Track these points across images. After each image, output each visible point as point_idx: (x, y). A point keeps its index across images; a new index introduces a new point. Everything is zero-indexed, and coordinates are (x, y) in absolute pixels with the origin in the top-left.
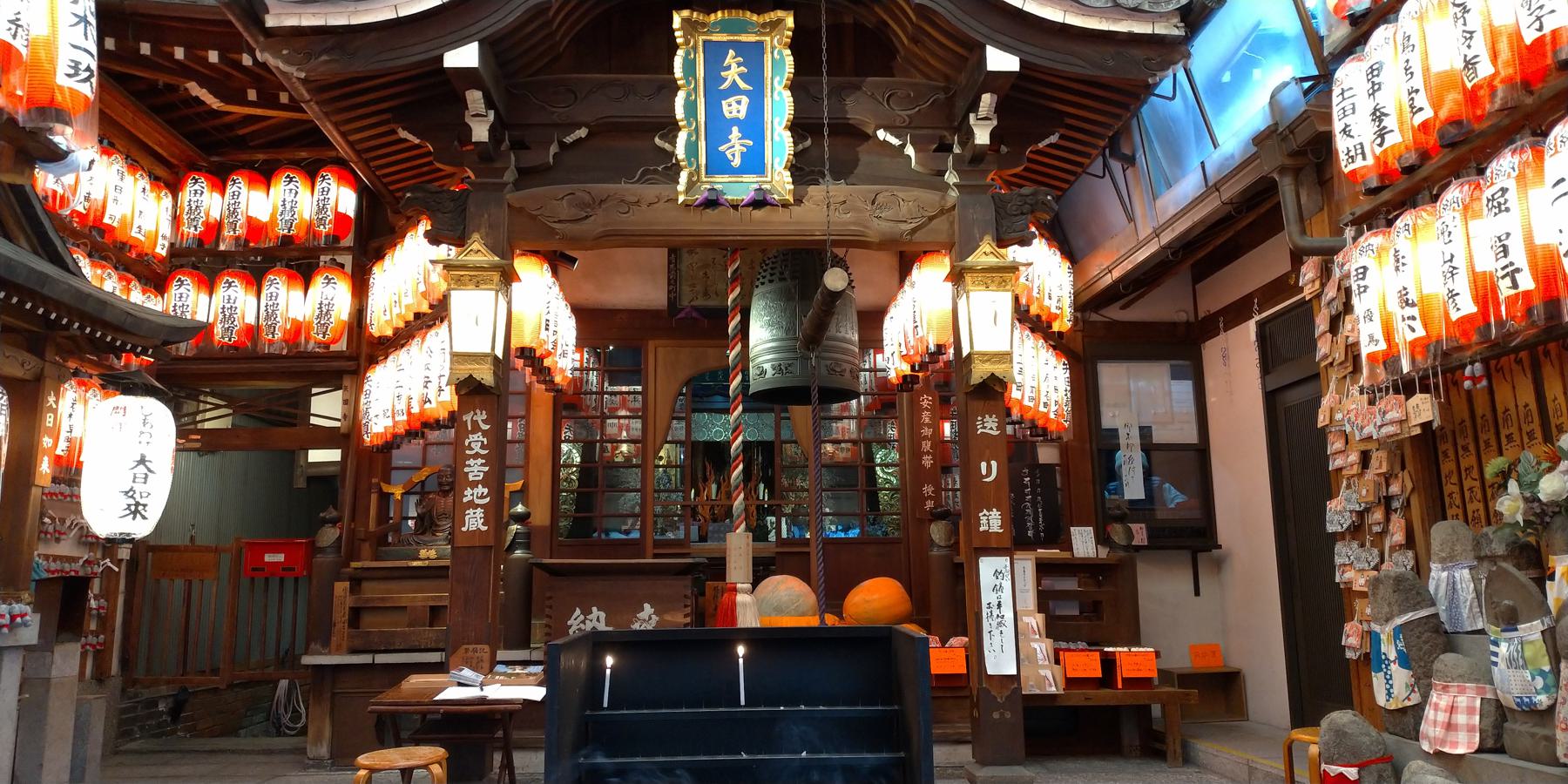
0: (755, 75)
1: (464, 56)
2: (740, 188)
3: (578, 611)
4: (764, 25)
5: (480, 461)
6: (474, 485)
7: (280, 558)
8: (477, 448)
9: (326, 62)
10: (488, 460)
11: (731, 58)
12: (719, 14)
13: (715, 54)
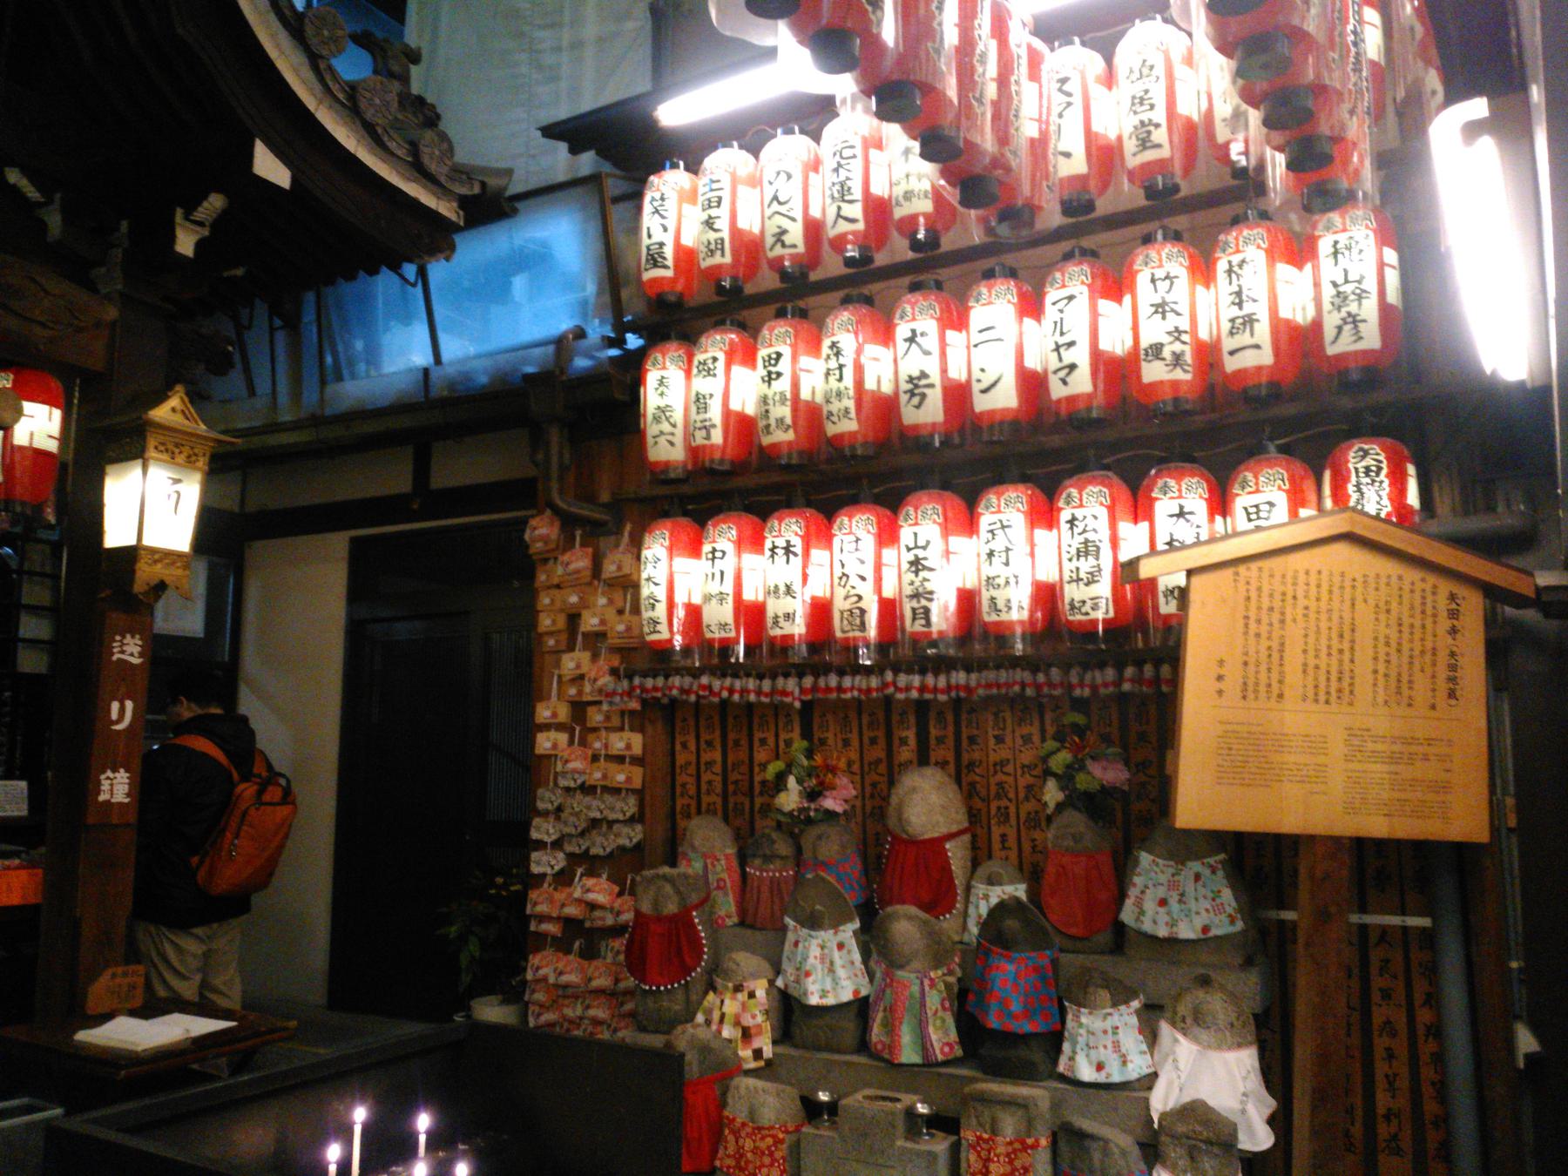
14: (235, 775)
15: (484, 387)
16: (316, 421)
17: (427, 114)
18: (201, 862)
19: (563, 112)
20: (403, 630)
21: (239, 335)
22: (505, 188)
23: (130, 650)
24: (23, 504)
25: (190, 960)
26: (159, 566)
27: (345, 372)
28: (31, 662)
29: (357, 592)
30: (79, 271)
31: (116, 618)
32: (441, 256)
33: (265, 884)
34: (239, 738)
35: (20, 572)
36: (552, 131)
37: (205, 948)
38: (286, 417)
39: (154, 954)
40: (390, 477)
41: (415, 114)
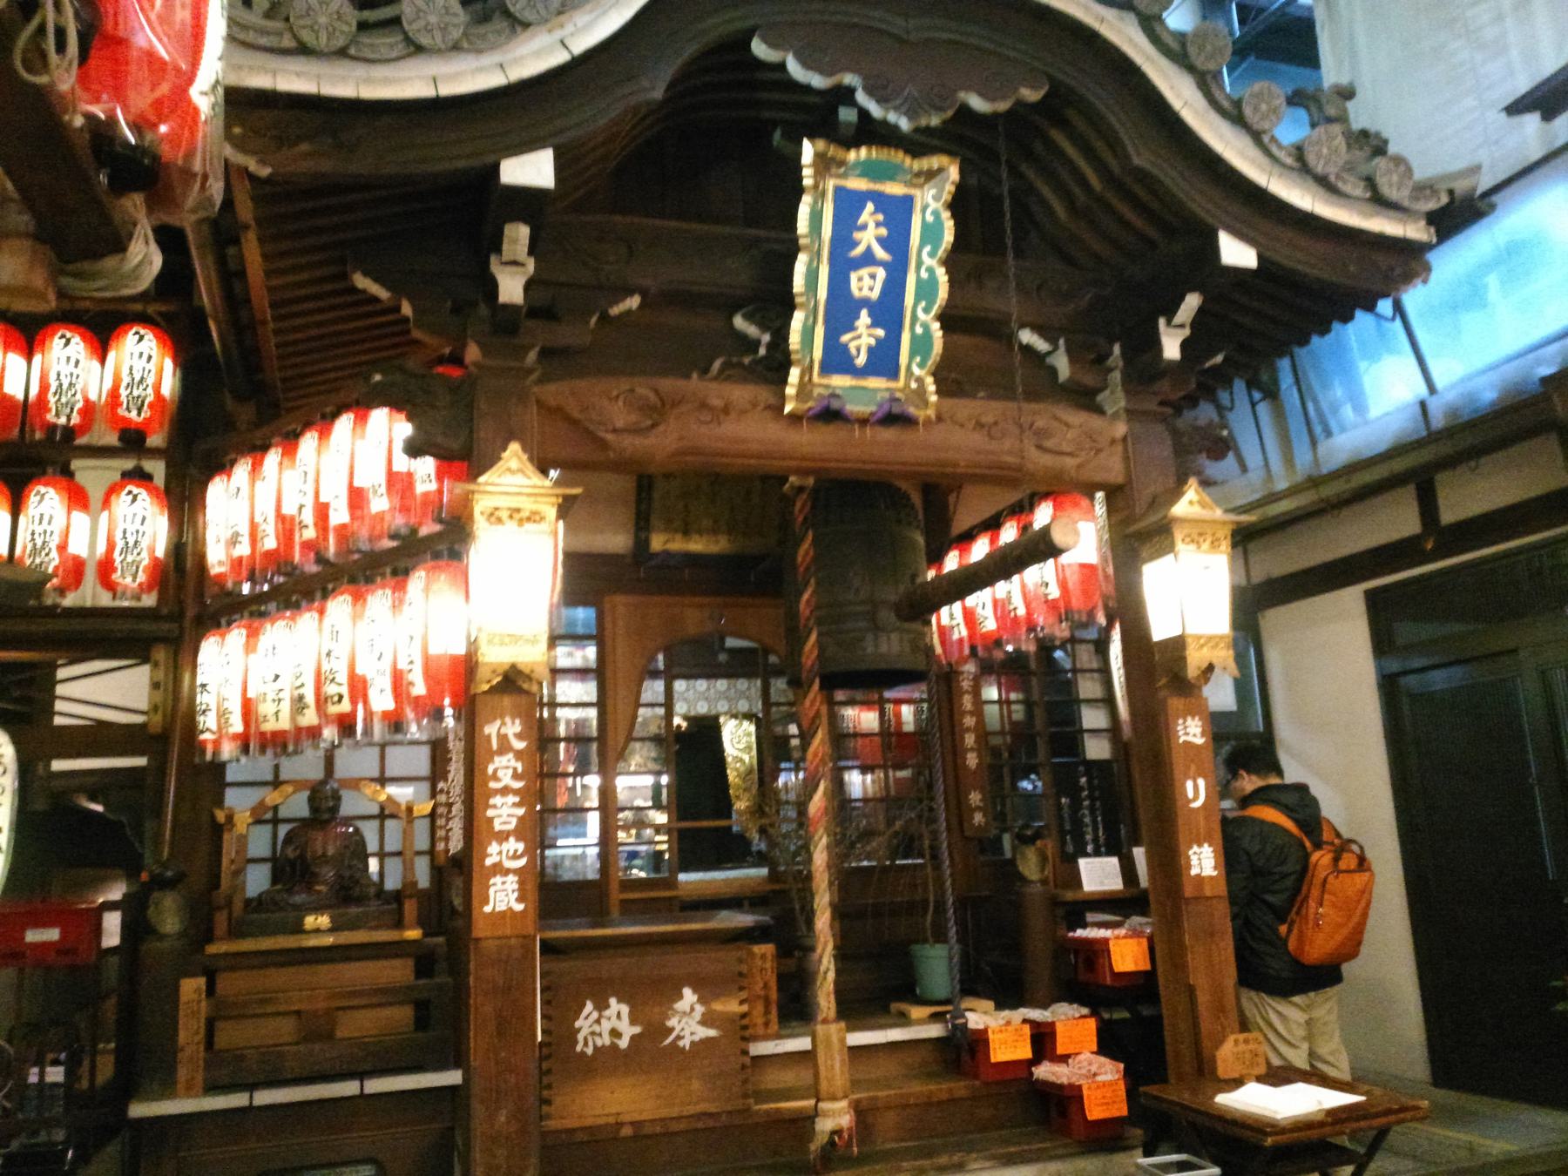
0: (897, 242)
1: (532, 169)
2: (863, 393)
3: (589, 1006)
4: (918, 174)
5: (512, 799)
6: (502, 837)
7: (53, 934)
8: (506, 779)
9: (306, 156)
10: (525, 797)
11: (868, 214)
12: (863, 151)
13: (849, 205)
14: (1308, 844)
15: (1493, 403)
16: (1314, 482)
17: (1372, 144)
18: (1290, 931)
19: (1523, 84)
20: (1439, 680)
21: (1222, 417)
22: (1474, 189)
23: (1191, 731)
24: (1079, 612)
25: (1294, 1026)
26: (1205, 649)
27: (1333, 424)
28: (1097, 749)
29: (1382, 644)
30: (1084, 397)
31: (1175, 703)
32: (1418, 281)
33: (1353, 954)
34: (1300, 802)
35: (1075, 671)
36: (1516, 108)
37: (1306, 1017)
38: (1282, 485)
39: (1262, 1023)
40: (1399, 520)
41: (1361, 149)
